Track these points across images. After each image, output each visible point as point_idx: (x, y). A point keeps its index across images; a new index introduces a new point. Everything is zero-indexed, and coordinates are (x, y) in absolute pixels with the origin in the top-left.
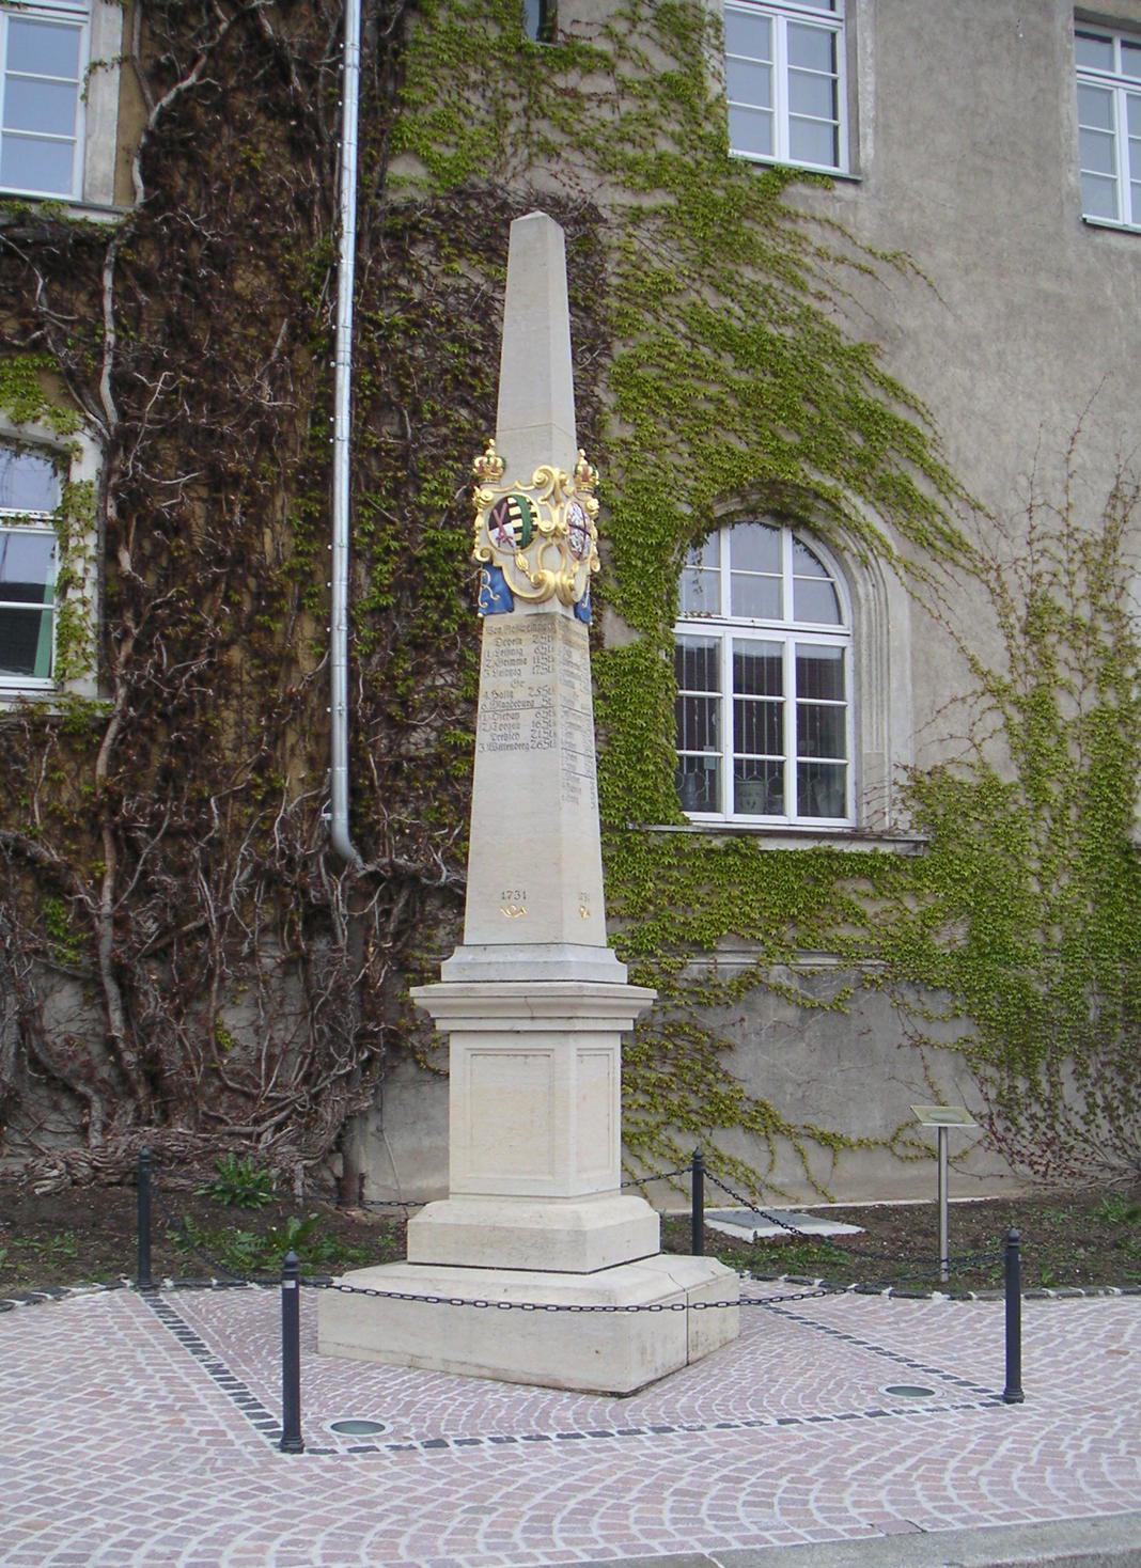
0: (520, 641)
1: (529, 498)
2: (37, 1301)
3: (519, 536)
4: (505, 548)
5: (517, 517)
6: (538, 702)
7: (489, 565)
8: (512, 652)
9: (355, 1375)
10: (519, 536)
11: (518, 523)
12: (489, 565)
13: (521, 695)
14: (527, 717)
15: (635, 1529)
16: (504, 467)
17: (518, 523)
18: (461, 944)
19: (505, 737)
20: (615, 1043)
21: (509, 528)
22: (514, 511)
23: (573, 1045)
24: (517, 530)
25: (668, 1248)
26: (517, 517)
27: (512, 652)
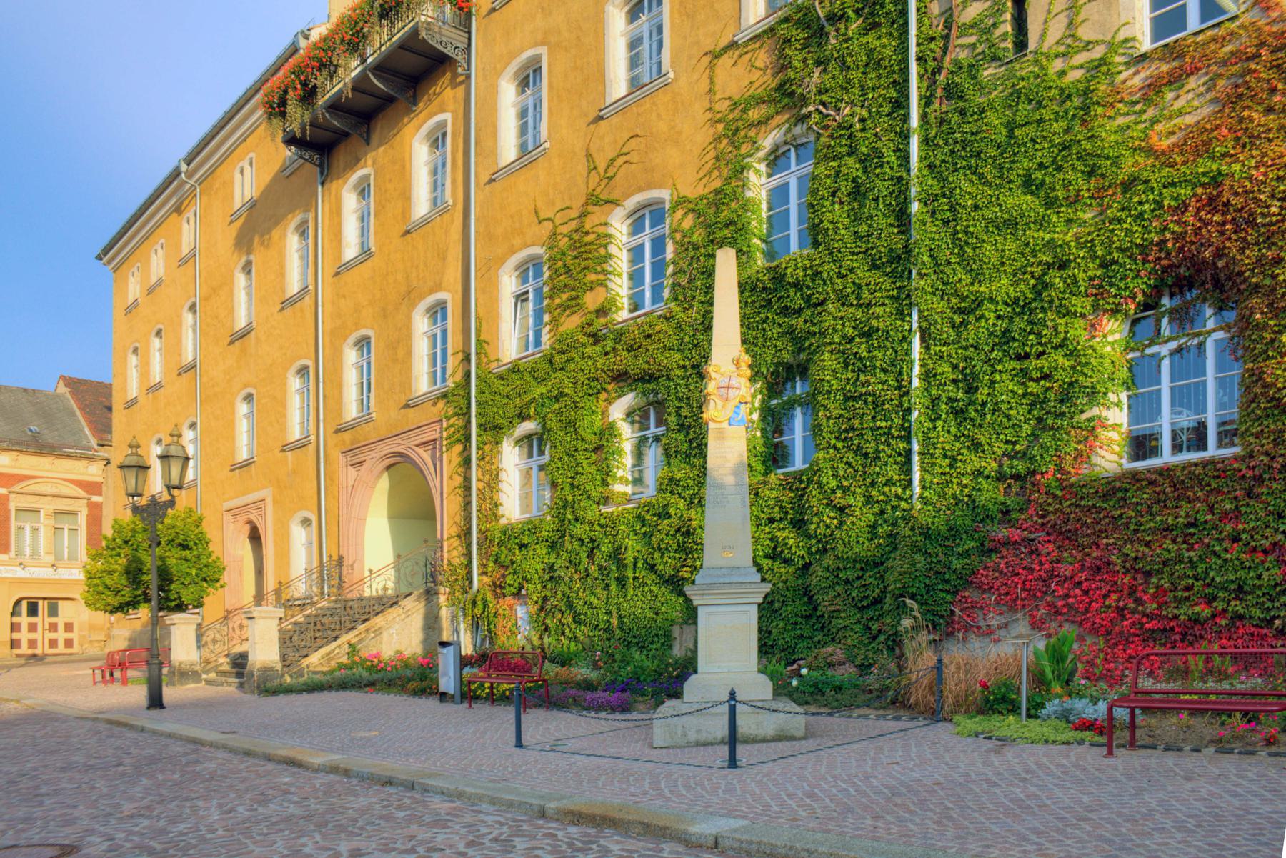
20: (755, 609)
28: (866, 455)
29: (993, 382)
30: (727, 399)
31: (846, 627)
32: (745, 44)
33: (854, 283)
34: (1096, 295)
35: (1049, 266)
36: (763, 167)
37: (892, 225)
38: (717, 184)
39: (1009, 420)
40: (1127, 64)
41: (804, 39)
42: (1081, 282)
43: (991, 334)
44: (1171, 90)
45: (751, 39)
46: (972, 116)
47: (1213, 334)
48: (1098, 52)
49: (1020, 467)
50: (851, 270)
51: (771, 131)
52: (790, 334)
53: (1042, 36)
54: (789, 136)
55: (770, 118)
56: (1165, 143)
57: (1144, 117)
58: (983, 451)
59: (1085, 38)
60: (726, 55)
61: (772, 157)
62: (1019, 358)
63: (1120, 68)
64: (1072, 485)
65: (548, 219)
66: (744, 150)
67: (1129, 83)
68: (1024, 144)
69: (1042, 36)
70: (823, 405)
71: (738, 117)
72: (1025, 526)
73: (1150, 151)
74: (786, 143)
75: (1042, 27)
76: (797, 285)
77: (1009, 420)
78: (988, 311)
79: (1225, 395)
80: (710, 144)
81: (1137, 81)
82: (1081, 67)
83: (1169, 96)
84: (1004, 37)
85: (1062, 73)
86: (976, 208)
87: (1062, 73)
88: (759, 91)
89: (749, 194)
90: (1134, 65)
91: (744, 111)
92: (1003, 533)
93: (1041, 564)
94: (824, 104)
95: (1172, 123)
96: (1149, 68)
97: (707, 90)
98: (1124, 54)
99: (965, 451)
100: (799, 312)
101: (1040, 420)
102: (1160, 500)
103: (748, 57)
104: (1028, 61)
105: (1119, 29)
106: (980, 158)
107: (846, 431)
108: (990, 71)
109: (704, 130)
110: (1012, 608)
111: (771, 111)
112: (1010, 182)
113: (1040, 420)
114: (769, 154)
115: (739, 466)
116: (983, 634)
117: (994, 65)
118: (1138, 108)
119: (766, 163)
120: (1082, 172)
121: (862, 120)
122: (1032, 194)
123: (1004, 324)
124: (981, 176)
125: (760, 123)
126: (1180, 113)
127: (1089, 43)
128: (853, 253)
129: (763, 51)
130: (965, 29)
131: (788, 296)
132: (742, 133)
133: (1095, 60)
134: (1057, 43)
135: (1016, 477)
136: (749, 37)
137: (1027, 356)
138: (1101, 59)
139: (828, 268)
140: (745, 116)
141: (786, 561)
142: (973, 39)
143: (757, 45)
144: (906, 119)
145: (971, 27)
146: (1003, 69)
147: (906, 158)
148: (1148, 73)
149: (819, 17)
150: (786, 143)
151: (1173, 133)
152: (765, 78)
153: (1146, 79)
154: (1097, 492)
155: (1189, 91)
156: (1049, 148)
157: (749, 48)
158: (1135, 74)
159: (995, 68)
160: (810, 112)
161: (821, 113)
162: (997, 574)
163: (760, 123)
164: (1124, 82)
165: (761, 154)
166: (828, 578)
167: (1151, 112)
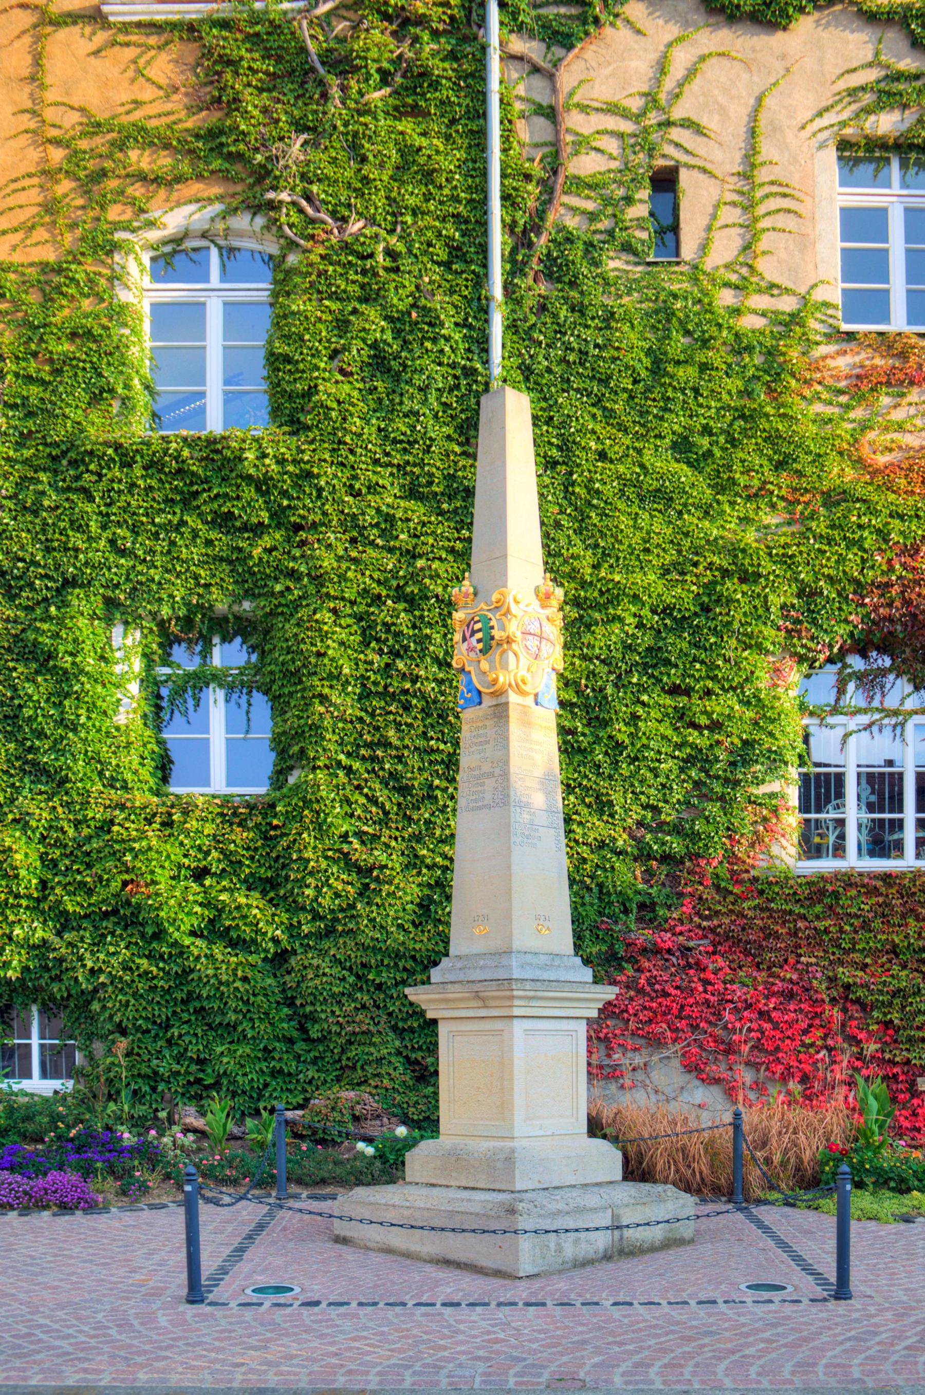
0: (485, 727)
1: (490, 615)
2: (90, 1206)
3: (480, 646)
4: (472, 654)
5: (480, 630)
6: (497, 771)
7: (462, 670)
8: (479, 736)
9: (747, 1335)
10: (480, 646)
11: (479, 635)
12: (462, 670)
13: (486, 768)
14: (490, 783)
15: (308, 1322)
16: (475, 594)
17: (479, 635)
18: (447, 955)
19: (476, 800)
20: (582, 1028)
21: (473, 640)
22: (478, 626)
23: (519, 1027)
24: (479, 641)
25: (625, 1178)
26: (480, 630)
27: (479, 736)
28: (405, 790)
29: (635, 717)
30: (537, 657)
31: (379, 1061)
32: (125, 28)
33: (378, 510)
34: (788, 631)
35: (726, 573)
36: (146, 257)
37: (449, 438)
38: (50, 255)
39: (656, 776)
40: (828, 337)
41: (267, 73)
42: (773, 609)
43: (629, 648)
44: (887, 394)
45: (139, 25)
46: (593, 318)
47: (915, 717)
48: (788, 304)
49: (676, 845)
50: (373, 488)
51: (179, 204)
52: (230, 562)
53: (704, 247)
54: (220, 226)
55: (179, 179)
56: (882, 459)
57: (852, 415)
58: (612, 815)
59: (768, 277)
60: (76, 30)
61: (168, 249)
62: (674, 691)
63: (818, 338)
64: (756, 879)
65: (716, 207)
66: (114, 213)
67: (831, 363)
68: (683, 390)
69: (704, 247)
70: (321, 695)
71: (104, 150)
72: (678, 929)
73: (860, 463)
74: (204, 235)
75: (703, 234)
76: (263, 485)
77: (656, 776)
78: (627, 611)
79: (873, 793)
80: (30, 175)
81: (843, 363)
82: (763, 315)
83: (885, 400)
84: (640, 223)
85: (736, 312)
86: (602, 456)
87: (736, 312)
88: (154, 123)
89: (124, 296)
90: (837, 342)
91: (121, 145)
92: (644, 936)
93: (706, 982)
94: (308, 198)
95: (888, 437)
96: (858, 353)
97: (26, 73)
98: (823, 322)
99: (585, 811)
100: (258, 529)
101: (697, 784)
102: (884, 912)
103: (131, 52)
104: (682, 273)
105: (816, 285)
106: (607, 387)
107: (369, 745)
108: (616, 264)
109: (13, 143)
110: (656, 1042)
111: (185, 167)
112: (659, 436)
113: (697, 784)
114: (165, 243)
115: (547, 778)
116: (608, 1077)
117: (624, 256)
118: (843, 399)
119: (152, 254)
120: (770, 460)
121: (390, 253)
122: (689, 464)
123: (647, 640)
124: (609, 414)
125: (157, 180)
126: (900, 428)
127: (772, 286)
128: (376, 462)
129: (164, 57)
130: (579, 184)
131: (238, 498)
132: (112, 184)
133: (783, 313)
134: (727, 267)
135: (666, 858)
136: (135, 18)
137: (688, 692)
138: (792, 315)
139: (327, 474)
140: (119, 155)
141: (237, 944)
142: (590, 206)
143: (153, 40)
144: (480, 280)
145: (590, 187)
146: (640, 269)
147: (482, 344)
148: (857, 359)
149: (303, 50)
150: (204, 235)
151: (891, 450)
152: (169, 107)
153: (854, 366)
154: (795, 893)
155: (910, 404)
156: (718, 409)
157: (133, 38)
158: (838, 353)
159: (628, 263)
160: (281, 202)
161: (301, 211)
162: (632, 993)
163: (157, 180)
164: (824, 358)
165: (153, 235)
166: (343, 979)
167: (858, 414)
